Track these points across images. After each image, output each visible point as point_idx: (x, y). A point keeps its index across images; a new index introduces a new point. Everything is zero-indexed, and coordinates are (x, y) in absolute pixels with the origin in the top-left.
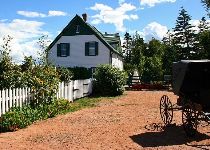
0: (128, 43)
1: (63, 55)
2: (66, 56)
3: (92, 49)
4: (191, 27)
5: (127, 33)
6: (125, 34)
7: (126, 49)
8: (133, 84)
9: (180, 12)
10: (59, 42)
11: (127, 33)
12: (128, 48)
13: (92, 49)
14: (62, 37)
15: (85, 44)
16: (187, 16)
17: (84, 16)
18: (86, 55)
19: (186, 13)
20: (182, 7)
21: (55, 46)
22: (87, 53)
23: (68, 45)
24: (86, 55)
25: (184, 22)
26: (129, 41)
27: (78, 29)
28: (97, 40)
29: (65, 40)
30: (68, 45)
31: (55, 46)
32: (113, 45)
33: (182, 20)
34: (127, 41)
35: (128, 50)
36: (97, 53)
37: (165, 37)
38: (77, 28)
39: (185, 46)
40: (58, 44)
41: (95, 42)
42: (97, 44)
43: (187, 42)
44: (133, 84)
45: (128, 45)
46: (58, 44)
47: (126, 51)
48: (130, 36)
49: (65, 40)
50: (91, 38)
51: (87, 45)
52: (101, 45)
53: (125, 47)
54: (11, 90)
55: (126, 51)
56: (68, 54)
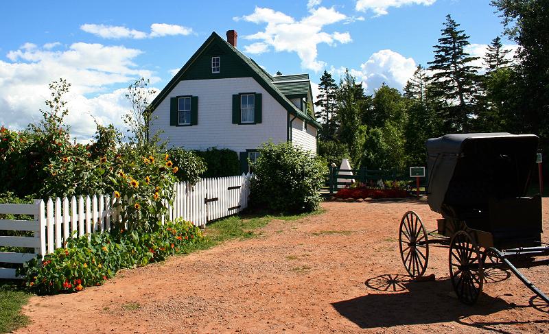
0: (328, 96)
1: (184, 122)
2: (189, 124)
3: (248, 110)
4: (470, 60)
5: (325, 73)
6: (323, 77)
7: (324, 108)
8: (339, 186)
9: (445, 27)
10: (174, 93)
11: (325, 73)
12: (328, 108)
13: (248, 110)
14: (181, 82)
15: (263, 120)
16: (461, 35)
17: (231, 35)
18: (234, 122)
19: (457, 29)
20: (449, 16)
21: (166, 103)
22: (237, 119)
23: (194, 101)
24: (234, 122)
25: (454, 48)
26: (330, 91)
27: (218, 64)
28: (259, 89)
29: (187, 88)
30: (194, 101)
31: (166, 103)
32: (295, 100)
33: (448, 45)
34: (327, 92)
35: (328, 112)
36: (258, 119)
37: (411, 81)
38: (215, 62)
39: (456, 102)
40: (172, 99)
41: (254, 93)
42: (258, 98)
43: (460, 93)
44: (339, 186)
45: (327, 100)
46: (172, 99)
47: (324, 113)
48: (333, 81)
49: (187, 88)
50: (246, 85)
51: (237, 100)
52: (267, 99)
53: (322, 106)
54: (66, 201)
55: (324, 113)
56: (194, 121)
